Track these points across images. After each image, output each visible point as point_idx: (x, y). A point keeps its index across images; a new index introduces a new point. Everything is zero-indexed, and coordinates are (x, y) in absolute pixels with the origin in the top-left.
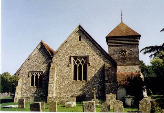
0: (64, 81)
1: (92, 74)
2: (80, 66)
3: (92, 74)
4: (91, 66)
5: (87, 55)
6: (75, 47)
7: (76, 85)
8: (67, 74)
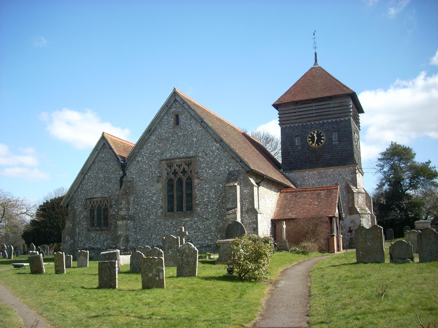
0: (149, 215)
1: (203, 196)
2: (180, 180)
3: (203, 196)
4: (202, 180)
5: (191, 153)
6: (167, 139)
7: (171, 223)
8: (154, 199)
